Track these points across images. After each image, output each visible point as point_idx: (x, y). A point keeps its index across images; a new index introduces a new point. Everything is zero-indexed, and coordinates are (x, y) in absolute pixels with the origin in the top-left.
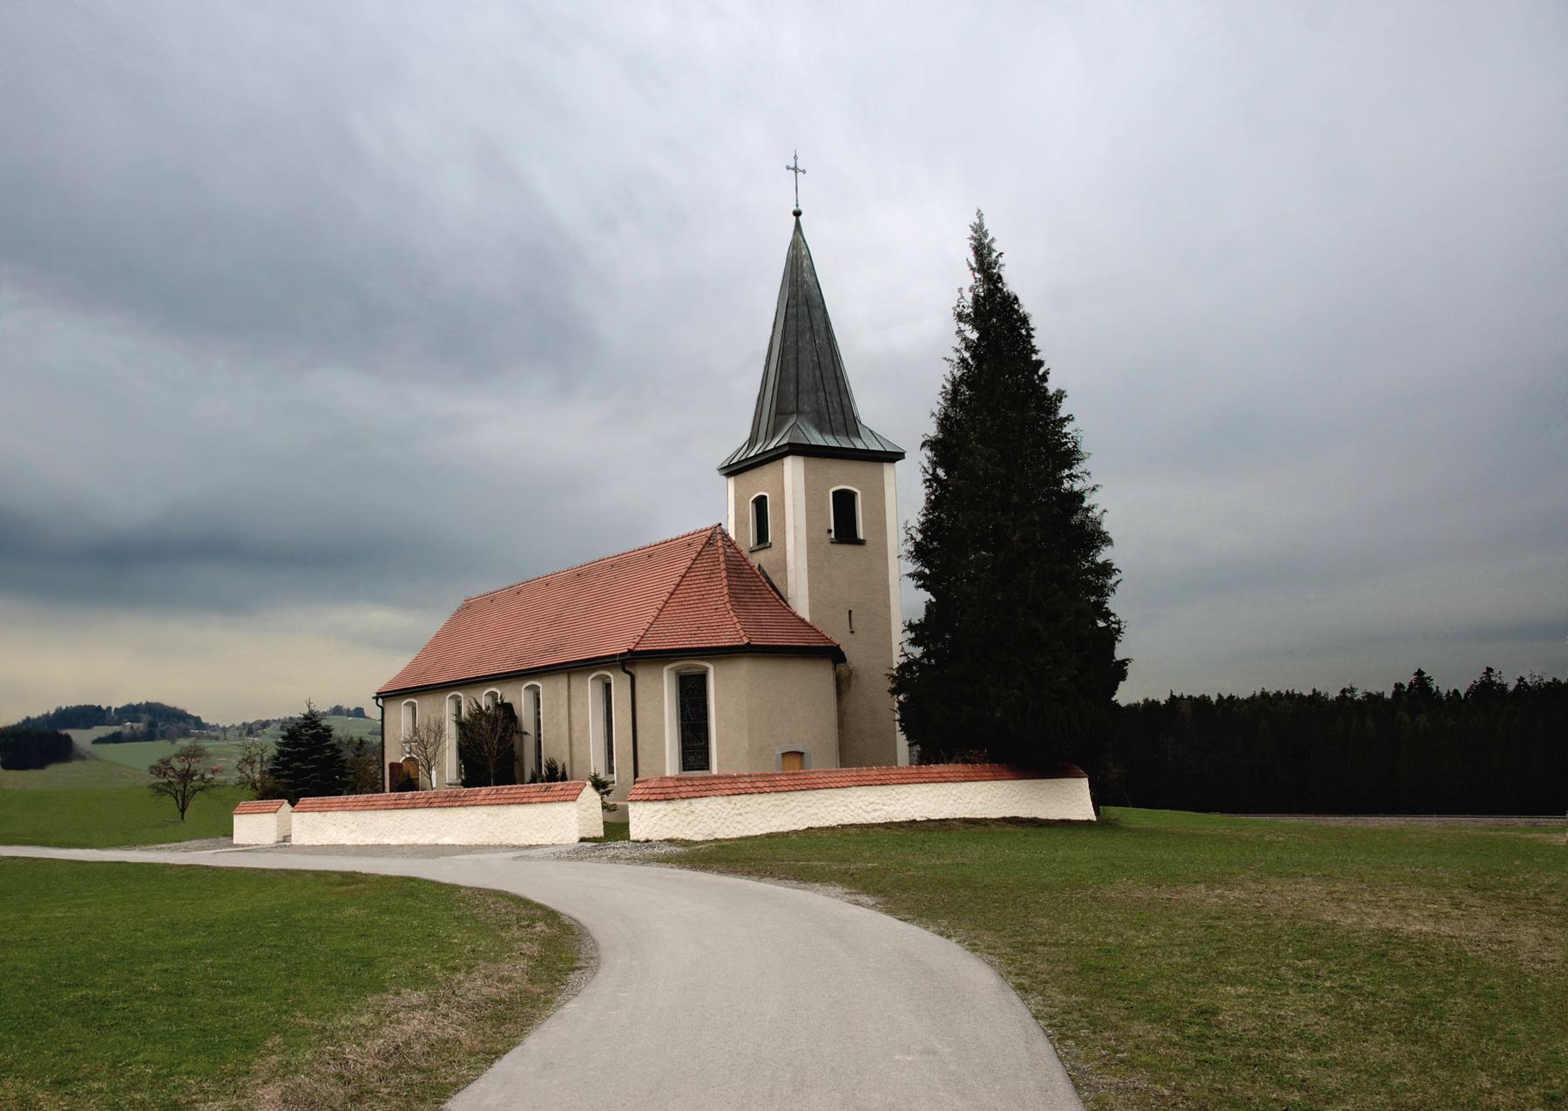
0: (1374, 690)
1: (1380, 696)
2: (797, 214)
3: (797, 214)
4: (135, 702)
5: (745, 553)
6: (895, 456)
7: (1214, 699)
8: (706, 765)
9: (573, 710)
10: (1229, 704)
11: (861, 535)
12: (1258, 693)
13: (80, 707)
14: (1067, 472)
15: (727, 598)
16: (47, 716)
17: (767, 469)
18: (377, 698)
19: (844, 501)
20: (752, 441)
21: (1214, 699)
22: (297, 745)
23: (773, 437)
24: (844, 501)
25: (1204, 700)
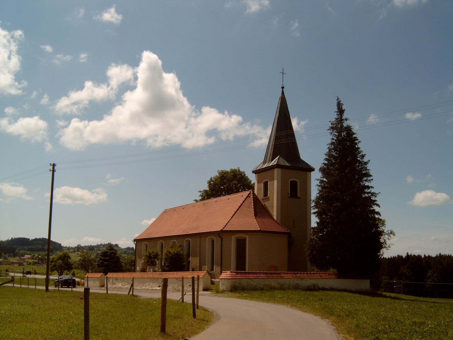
0: (401, 255)
1: (402, 257)
2: (283, 88)
3: (283, 88)
4: (38, 237)
5: (260, 200)
6: (313, 170)
7: (423, 256)
8: (245, 270)
9: (224, 243)
10: (429, 258)
11: (299, 195)
12: (438, 254)
13: (19, 238)
14: (365, 178)
15: (253, 215)
16: (8, 240)
17: (269, 172)
18: (134, 241)
19: (294, 185)
20: (264, 162)
21: (423, 256)
22: (107, 256)
23: (272, 160)
24: (294, 185)
25: (419, 257)
